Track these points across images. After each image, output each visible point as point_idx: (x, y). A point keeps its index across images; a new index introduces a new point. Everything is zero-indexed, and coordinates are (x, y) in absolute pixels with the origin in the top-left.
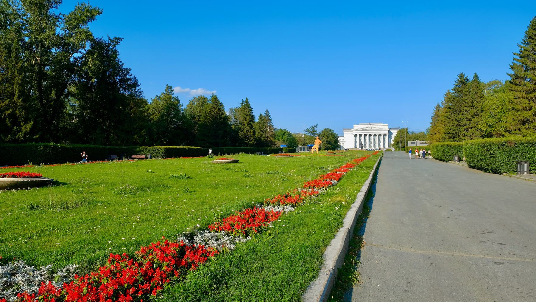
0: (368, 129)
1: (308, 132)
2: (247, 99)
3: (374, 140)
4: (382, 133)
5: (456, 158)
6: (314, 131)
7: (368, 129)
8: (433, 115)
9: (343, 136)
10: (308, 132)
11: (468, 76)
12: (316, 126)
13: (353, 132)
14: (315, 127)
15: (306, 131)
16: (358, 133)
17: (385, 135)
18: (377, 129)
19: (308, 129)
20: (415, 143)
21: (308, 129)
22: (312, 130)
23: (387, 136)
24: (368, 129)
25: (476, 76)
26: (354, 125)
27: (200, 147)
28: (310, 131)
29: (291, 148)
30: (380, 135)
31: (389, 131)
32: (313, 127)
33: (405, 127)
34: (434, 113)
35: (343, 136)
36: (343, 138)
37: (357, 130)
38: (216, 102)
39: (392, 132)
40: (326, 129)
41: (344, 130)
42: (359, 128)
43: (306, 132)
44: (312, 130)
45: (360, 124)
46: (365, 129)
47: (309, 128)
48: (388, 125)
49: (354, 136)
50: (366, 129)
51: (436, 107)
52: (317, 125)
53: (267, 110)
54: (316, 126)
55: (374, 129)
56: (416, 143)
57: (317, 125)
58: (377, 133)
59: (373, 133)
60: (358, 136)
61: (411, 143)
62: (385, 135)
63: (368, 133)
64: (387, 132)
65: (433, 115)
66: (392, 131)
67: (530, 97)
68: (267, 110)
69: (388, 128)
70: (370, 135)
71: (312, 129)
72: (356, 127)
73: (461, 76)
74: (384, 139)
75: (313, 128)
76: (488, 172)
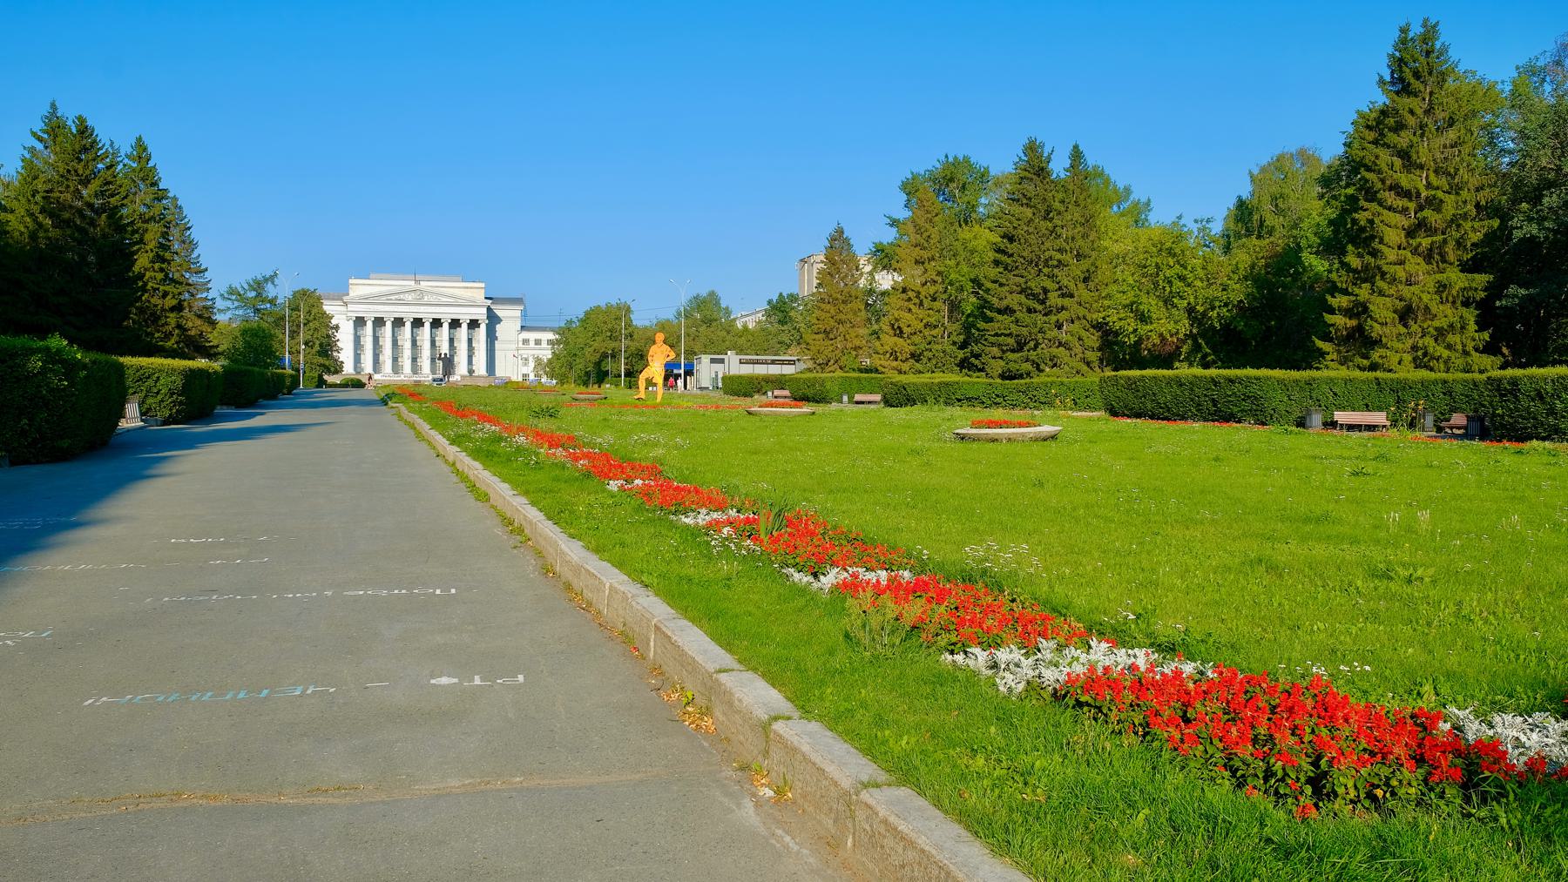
0: (409, 298)
1: (236, 304)
3: (393, 341)
4: (465, 315)
7: (410, 298)
10: (236, 304)
11: (1053, 151)
12: (271, 279)
13: (351, 307)
14: (266, 280)
15: (226, 295)
16: (370, 312)
17: (473, 324)
18: (444, 299)
20: (722, 361)
23: (483, 327)
24: (409, 298)
25: (140, 145)
30: (455, 324)
31: (489, 309)
33: (704, 293)
37: (365, 300)
39: (499, 313)
44: (253, 294)
48: (483, 285)
49: (351, 323)
54: (271, 279)
55: (433, 299)
56: (726, 361)
58: (446, 314)
59: (427, 314)
60: (369, 325)
61: (713, 361)
62: (473, 324)
63: (408, 313)
64: (480, 314)
66: (500, 311)
67: (1059, 213)
69: (486, 298)
70: (418, 323)
73: (1032, 148)
74: (376, 339)
75: (258, 286)
76: (861, 549)
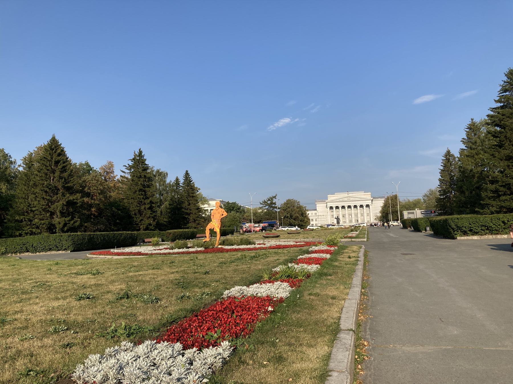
0: (346, 199)
2: (141, 152)
5: (10, 202)
6: (272, 203)
8: (442, 168)
9: (316, 210)
16: (334, 205)
19: (264, 200)
20: (413, 213)
21: (264, 200)
22: (269, 202)
26: (328, 196)
27: (131, 231)
28: (268, 203)
29: (103, 233)
32: (271, 198)
34: (442, 164)
35: (316, 210)
36: (315, 212)
37: (332, 202)
38: (53, 149)
40: (289, 201)
41: (316, 202)
42: (334, 199)
43: (262, 206)
45: (336, 193)
46: (342, 199)
47: (266, 199)
48: (370, 193)
50: (343, 199)
51: (446, 156)
52: (276, 195)
53: (187, 171)
54: (275, 197)
57: (276, 195)
61: (409, 213)
65: (442, 168)
68: (187, 171)
71: (269, 200)
72: (331, 198)
75: (271, 199)
